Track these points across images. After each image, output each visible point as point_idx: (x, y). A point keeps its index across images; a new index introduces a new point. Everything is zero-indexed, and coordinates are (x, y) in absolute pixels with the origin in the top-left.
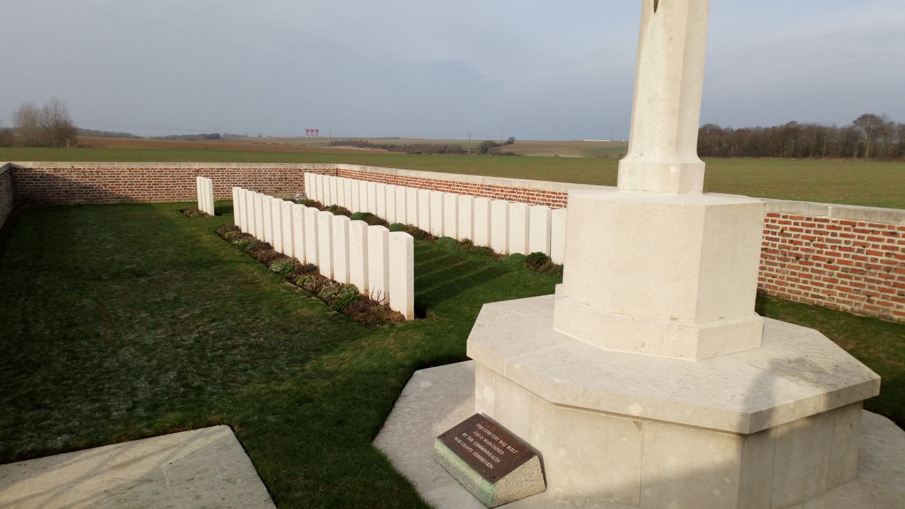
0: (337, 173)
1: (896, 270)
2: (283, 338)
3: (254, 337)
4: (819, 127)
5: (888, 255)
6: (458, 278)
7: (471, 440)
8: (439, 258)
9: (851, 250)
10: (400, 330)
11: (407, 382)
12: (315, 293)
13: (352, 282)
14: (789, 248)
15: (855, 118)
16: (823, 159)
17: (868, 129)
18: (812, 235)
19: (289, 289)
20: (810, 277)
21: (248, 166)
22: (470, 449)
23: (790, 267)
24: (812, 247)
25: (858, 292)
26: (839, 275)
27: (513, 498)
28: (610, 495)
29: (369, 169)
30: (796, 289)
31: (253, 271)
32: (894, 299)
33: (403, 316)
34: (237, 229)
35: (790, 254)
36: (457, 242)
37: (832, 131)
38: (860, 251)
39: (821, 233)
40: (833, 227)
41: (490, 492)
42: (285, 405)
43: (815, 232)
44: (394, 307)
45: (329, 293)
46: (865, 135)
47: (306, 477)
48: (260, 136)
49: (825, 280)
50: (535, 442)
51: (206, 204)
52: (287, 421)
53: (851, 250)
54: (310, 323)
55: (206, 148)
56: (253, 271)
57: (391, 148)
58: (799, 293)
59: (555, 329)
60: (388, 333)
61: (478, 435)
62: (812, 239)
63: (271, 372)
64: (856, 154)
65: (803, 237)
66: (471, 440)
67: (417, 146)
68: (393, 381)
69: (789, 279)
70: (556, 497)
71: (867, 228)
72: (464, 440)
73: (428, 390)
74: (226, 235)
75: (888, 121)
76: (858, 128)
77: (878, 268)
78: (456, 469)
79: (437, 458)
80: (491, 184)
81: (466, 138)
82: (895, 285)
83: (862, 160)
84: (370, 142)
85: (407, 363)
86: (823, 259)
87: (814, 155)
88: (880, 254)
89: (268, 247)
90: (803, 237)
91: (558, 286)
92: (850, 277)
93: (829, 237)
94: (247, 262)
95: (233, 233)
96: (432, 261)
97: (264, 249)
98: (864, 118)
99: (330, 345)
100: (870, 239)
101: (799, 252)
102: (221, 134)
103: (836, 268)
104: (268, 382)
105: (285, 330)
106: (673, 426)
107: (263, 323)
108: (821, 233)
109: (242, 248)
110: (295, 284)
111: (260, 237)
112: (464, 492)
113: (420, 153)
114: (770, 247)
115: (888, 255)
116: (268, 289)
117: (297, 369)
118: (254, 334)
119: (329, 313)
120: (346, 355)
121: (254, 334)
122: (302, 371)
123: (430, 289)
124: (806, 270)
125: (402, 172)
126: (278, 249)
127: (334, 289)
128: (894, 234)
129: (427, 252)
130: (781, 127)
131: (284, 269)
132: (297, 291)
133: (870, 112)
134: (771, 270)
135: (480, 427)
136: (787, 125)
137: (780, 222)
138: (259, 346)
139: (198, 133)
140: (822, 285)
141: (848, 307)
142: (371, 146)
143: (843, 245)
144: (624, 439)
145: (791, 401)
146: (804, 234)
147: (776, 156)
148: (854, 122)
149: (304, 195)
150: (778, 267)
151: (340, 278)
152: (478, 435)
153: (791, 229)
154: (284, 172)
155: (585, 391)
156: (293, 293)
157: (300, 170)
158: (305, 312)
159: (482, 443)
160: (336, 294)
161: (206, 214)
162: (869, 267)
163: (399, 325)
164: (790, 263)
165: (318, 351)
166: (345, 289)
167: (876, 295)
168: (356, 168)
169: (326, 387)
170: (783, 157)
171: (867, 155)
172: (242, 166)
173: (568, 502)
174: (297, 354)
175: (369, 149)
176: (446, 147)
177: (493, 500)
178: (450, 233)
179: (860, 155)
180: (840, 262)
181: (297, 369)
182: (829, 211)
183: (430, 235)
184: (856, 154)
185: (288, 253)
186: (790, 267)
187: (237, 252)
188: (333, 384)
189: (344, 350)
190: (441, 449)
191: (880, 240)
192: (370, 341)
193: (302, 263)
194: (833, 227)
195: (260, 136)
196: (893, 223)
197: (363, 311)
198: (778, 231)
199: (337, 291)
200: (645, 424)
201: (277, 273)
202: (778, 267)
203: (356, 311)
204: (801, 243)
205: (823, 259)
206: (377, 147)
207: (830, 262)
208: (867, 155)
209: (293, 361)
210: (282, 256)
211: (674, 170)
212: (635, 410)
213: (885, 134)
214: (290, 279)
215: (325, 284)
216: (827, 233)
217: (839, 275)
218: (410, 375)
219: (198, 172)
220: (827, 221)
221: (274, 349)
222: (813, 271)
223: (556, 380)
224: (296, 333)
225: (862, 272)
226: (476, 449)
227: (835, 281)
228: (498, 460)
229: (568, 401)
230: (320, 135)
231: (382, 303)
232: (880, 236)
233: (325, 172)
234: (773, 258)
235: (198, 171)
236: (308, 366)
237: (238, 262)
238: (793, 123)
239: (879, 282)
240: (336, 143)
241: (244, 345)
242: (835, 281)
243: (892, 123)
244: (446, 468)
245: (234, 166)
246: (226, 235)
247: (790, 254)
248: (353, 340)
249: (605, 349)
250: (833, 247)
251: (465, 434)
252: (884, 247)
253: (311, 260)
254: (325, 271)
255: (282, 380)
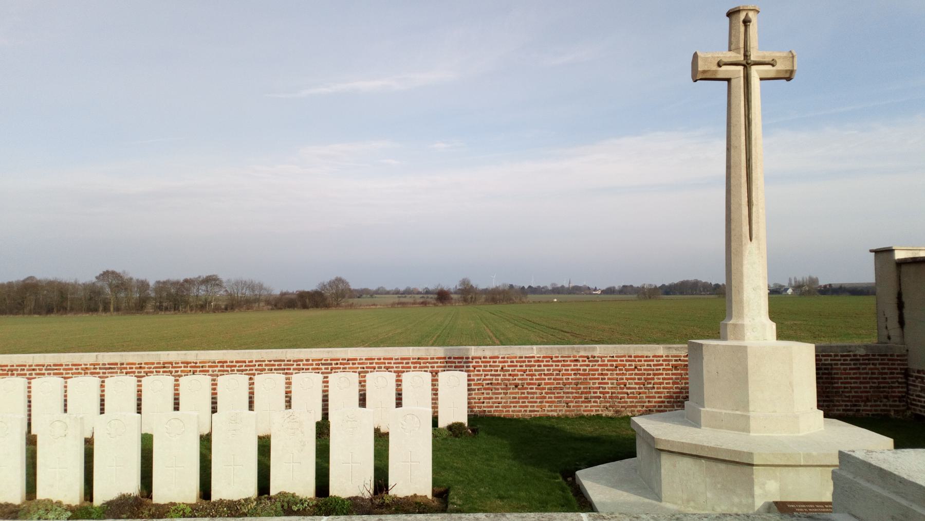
1: (581, 383)
4: (60, 283)
5: (575, 374)
9: (552, 374)
14: (509, 380)
15: (98, 275)
16: (69, 315)
17: (110, 285)
18: (524, 368)
20: (527, 398)
23: (511, 393)
24: (525, 377)
25: (560, 402)
26: (546, 393)
30: (518, 409)
32: (583, 402)
35: (510, 384)
37: (75, 287)
38: (557, 374)
39: (530, 366)
40: (538, 361)
43: (526, 366)
46: (108, 290)
49: (537, 398)
53: (552, 374)
58: (520, 411)
62: (525, 371)
64: (101, 308)
65: (518, 371)
69: (511, 402)
71: (560, 359)
75: (129, 276)
76: (99, 284)
77: (571, 383)
82: (582, 393)
83: (108, 314)
86: (534, 384)
87: (58, 311)
88: (570, 375)
90: (518, 371)
91: (822, 412)
92: (554, 393)
93: (536, 368)
98: (106, 274)
100: (563, 366)
101: (517, 381)
103: (544, 389)
108: (530, 366)
114: (494, 381)
115: (575, 374)
124: (523, 393)
128: (577, 361)
130: (18, 282)
133: (110, 269)
134: (497, 398)
136: (24, 281)
137: (500, 362)
140: (536, 402)
141: (555, 414)
143: (546, 372)
146: (518, 368)
147: (16, 314)
148: (530, 287)
150: (502, 395)
153: (509, 366)
162: (565, 384)
164: (511, 391)
167: (572, 402)
170: (24, 314)
171: (112, 309)
179: (106, 309)
180: (546, 384)
182: (535, 351)
184: (101, 308)
186: (511, 393)
191: (569, 365)
194: (538, 361)
196: (575, 354)
198: (499, 368)
202: (502, 395)
204: (517, 375)
205: (534, 384)
207: (539, 385)
208: (112, 309)
213: (126, 289)
216: (534, 366)
217: (546, 393)
220: (533, 357)
222: (528, 393)
225: (561, 389)
227: (545, 398)
232: (568, 363)
234: (498, 389)
238: (31, 278)
239: (572, 393)
242: (545, 398)
243: (131, 279)
247: (510, 384)
250: (540, 375)
252: (572, 370)
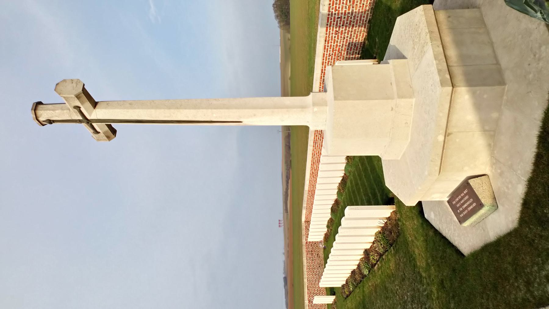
0: (308, 222)
2: (407, 283)
3: (408, 298)
6: (370, 173)
7: (461, 209)
8: (358, 177)
10: (401, 216)
11: (432, 225)
12: (381, 255)
13: (374, 234)
19: (379, 269)
21: (305, 273)
22: (466, 212)
27: (492, 194)
28: (489, 145)
29: (305, 205)
31: (368, 286)
33: (393, 211)
34: (343, 286)
36: (347, 164)
41: (488, 207)
42: (444, 295)
44: (388, 215)
45: (381, 248)
47: (483, 298)
48: (284, 254)
50: (461, 179)
51: (330, 299)
52: (453, 297)
54: (399, 264)
55: (293, 285)
56: (368, 286)
57: (288, 178)
59: (399, 159)
60: (403, 224)
61: (458, 205)
63: (427, 296)
66: (461, 209)
67: (286, 162)
68: (431, 233)
70: (491, 171)
72: (461, 212)
73: (435, 215)
74: (347, 293)
78: (477, 219)
79: (472, 226)
80: (312, 142)
81: (281, 133)
84: (285, 190)
85: (420, 221)
89: (353, 272)
94: (363, 287)
95: (346, 290)
96: (359, 182)
97: (355, 275)
99: (411, 259)
102: (284, 276)
104: (432, 299)
105: (403, 280)
106: (449, 119)
107: (399, 291)
109: (355, 287)
110: (375, 264)
111: (349, 275)
112: (490, 217)
113: (291, 161)
116: (379, 281)
117: (425, 281)
118: (406, 297)
119: (392, 252)
120: (417, 251)
121: (406, 297)
122: (426, 279)
123: (377, 190)
125: (306, 188)
126: (355, 267)
127: (378, 245)
129: (353, 182)
131: (367, 268)
132: (380, 265)
135: (454, 203)
138: (413, 297)
139: (284, 290)
142: (287, 189)
144: (457, 140)
145: (434, 61)
149: (321, 242)
151: (372, 239)
152: (458, 205)
154: (308, 252)
155: (432, 161)
156: (381, 267)
157: (306, 243)
158: (392, 265)
159: (463, 204)
160: (381, 244)
161: (334, 300)
163: (398, 216)
165: (415, 266)
166: (378, 239)
168: (304, 212)
169: (435, 270)
172: (305, 276)
173: (494, 166)
174: (416, 278)
175: (289, 191)
176: (286, 145)
177: (493, 206)
178: (343, 166)
181: (425, 281)
183: (343, 177)
185: (357, 263)
187: (357, 290)
188: (433, 265)
189: (414, 252)
190: (467, 224)
192: (408, 236)
193: (363, 256)
195: (284, 254)
197: (391, 233)
199: (379, 243)
200: (448, 131)
201: (369, 272)
203: (390, 235)
206: (287, 186)
209: (421, 281)
210: (359, 266)
211: (316, 109)
212: (441, 138)
214: (373, 266)
215: (375, 248)
218: (427, 222)
219: (310, 301)
221: (414, 290)
223: (426, 173)
224: (404, 274)
226: (466, 208)
228: (472, 200)
229: (437, 168)
230: (281, 218)
231: (386, 221)
233: (307, 229)
235: (309, 301)
236: (424, 275)
237: (363, 291)
240: (286, 210)
241: (412, 305)
244: (478, 223)
245: (305, 280)
246: (347, 293)
248: (408, 245)
249: (409, 140)
251: (459, 211)
253: (362, 252)
254: (368, 246)
255: (431, 291)
